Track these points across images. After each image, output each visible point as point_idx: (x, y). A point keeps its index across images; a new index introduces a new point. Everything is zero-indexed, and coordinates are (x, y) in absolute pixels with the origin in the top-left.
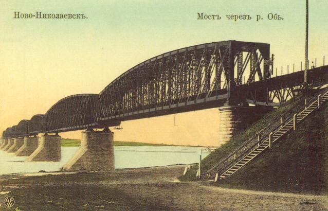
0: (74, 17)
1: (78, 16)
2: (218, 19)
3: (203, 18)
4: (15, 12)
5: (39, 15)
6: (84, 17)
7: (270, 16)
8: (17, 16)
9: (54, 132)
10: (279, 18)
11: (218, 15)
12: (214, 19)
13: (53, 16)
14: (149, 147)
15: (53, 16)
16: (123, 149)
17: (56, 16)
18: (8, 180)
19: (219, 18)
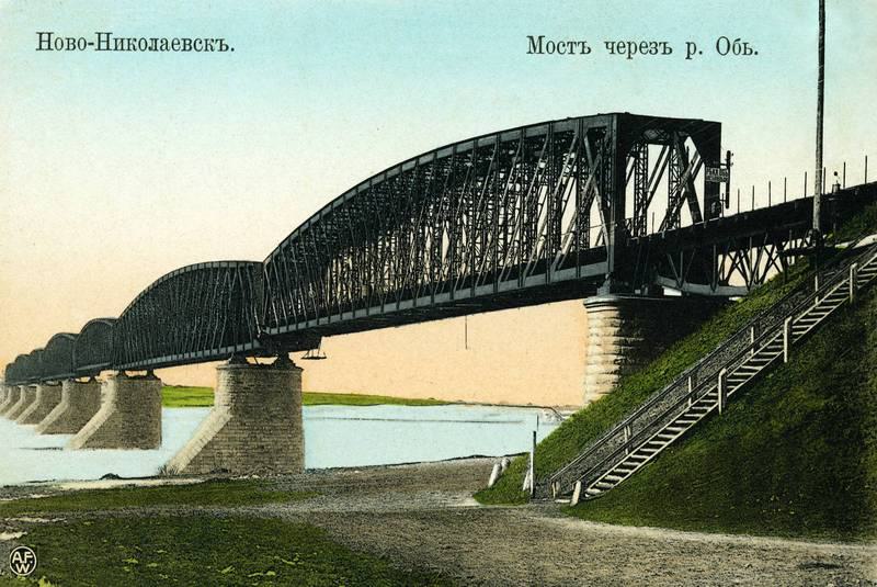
0: (198, 47)
1: (208, 47)
5: (104, 42)
6: (224, 47)
10: (746, 50)
17: (149, 44)
19: (586, 50)
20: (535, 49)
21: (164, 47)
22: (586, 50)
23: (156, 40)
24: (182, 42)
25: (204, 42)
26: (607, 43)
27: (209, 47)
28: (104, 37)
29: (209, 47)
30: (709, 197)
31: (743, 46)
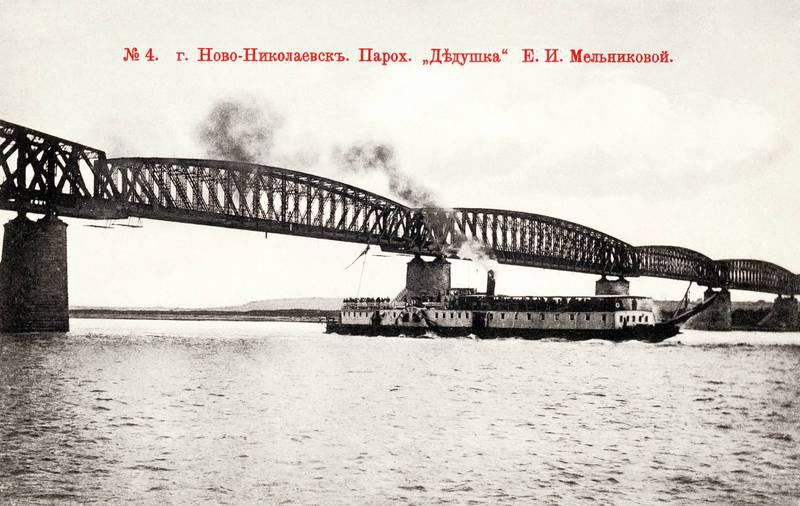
1: (329, 57)
4: (548, 51)
5: (251, 55)
17: (286, 56)
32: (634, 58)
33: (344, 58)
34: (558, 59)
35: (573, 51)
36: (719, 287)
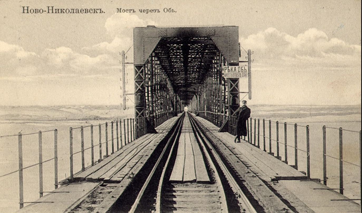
0: (91, 11)
1: (95, 11)
2: (133, 12)
3: (122, 11)
4: (24, 7)
5: (51, 10)
6: (101, 12)
7: (166, 10)
8: (26, 11)
9: (222, 97)
10: (173, 11)
11: (134, 10)
12: (130, 12)
13: (68, 11)
14: (252, 128)
15: (68, 11)
16: (268, 113)
17: (70, 11)
18: (162, 210)
19: (159, 11)
20: (119, 11)
21: (77, 12)
22: (159, 11)
23: (74, 9)
24: (84, 10)
25: (93, 10)
26: (140, 10)
27: (95, 12)
28: (50, 8)
29: (95, 12)
30: (222, 159)
31: (172, 10)
32: (64, 11)
33: (174, 11)
34: (99, 10)
35: (118, 9)
36: (240, 137)
